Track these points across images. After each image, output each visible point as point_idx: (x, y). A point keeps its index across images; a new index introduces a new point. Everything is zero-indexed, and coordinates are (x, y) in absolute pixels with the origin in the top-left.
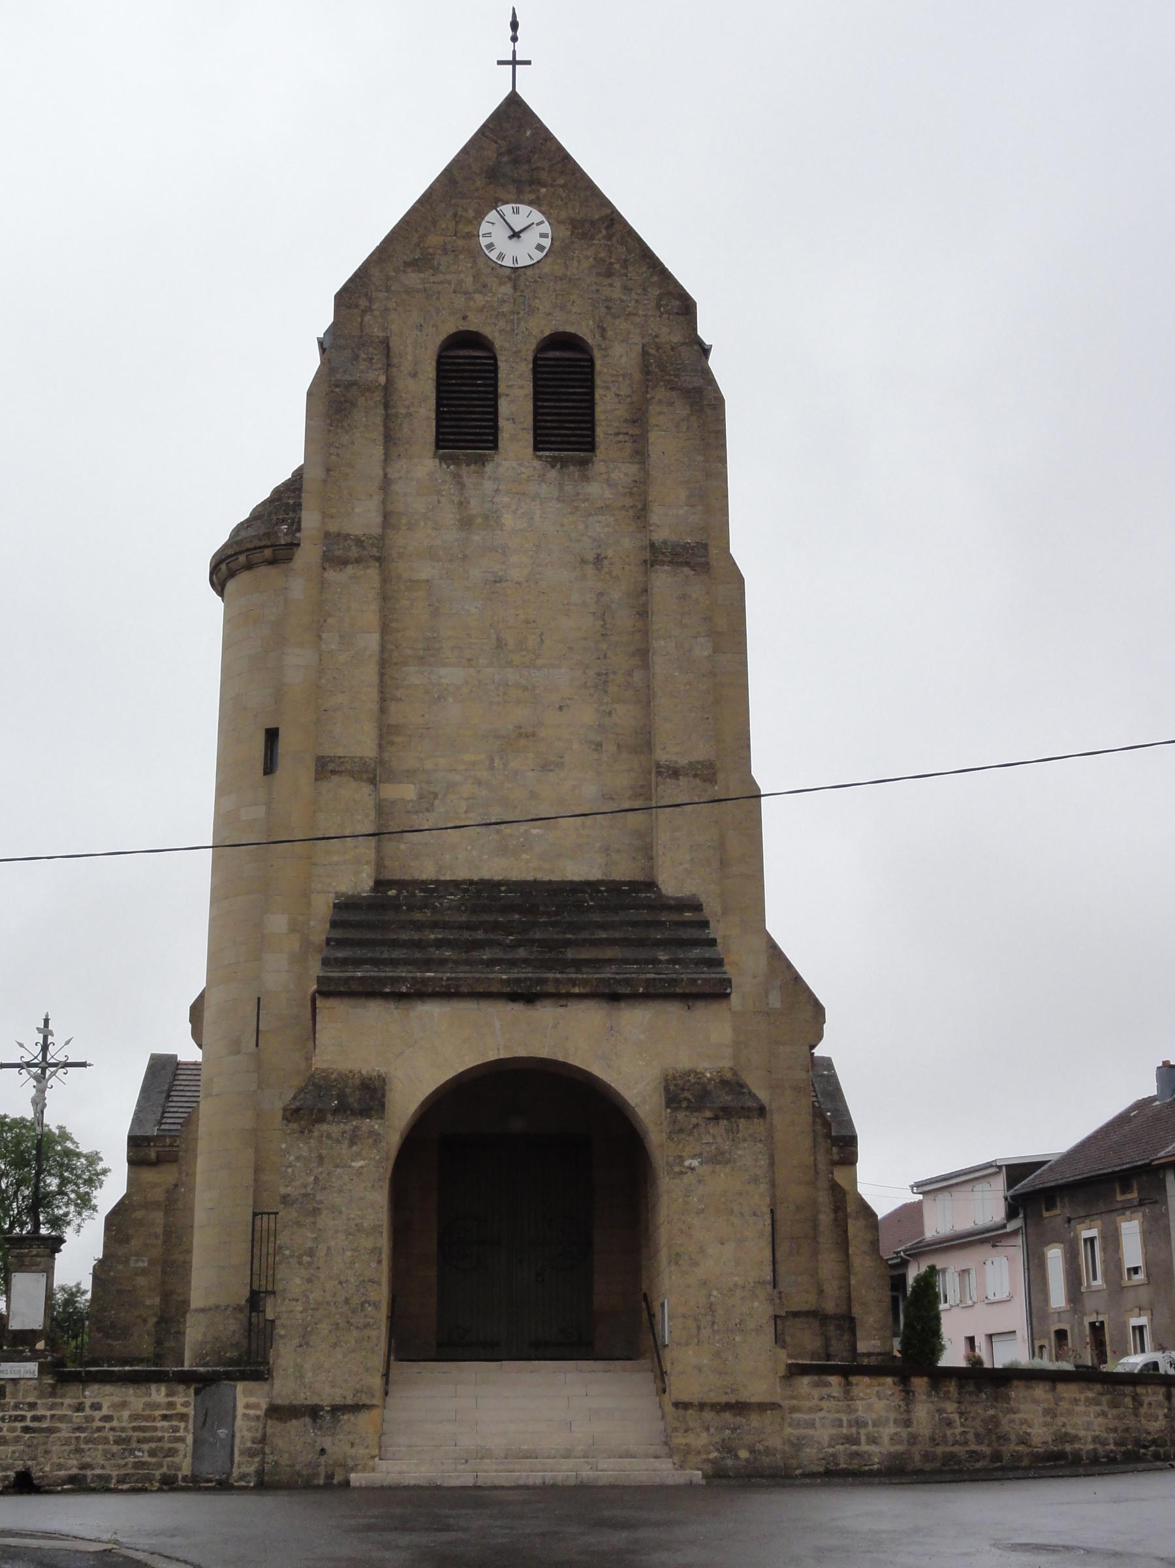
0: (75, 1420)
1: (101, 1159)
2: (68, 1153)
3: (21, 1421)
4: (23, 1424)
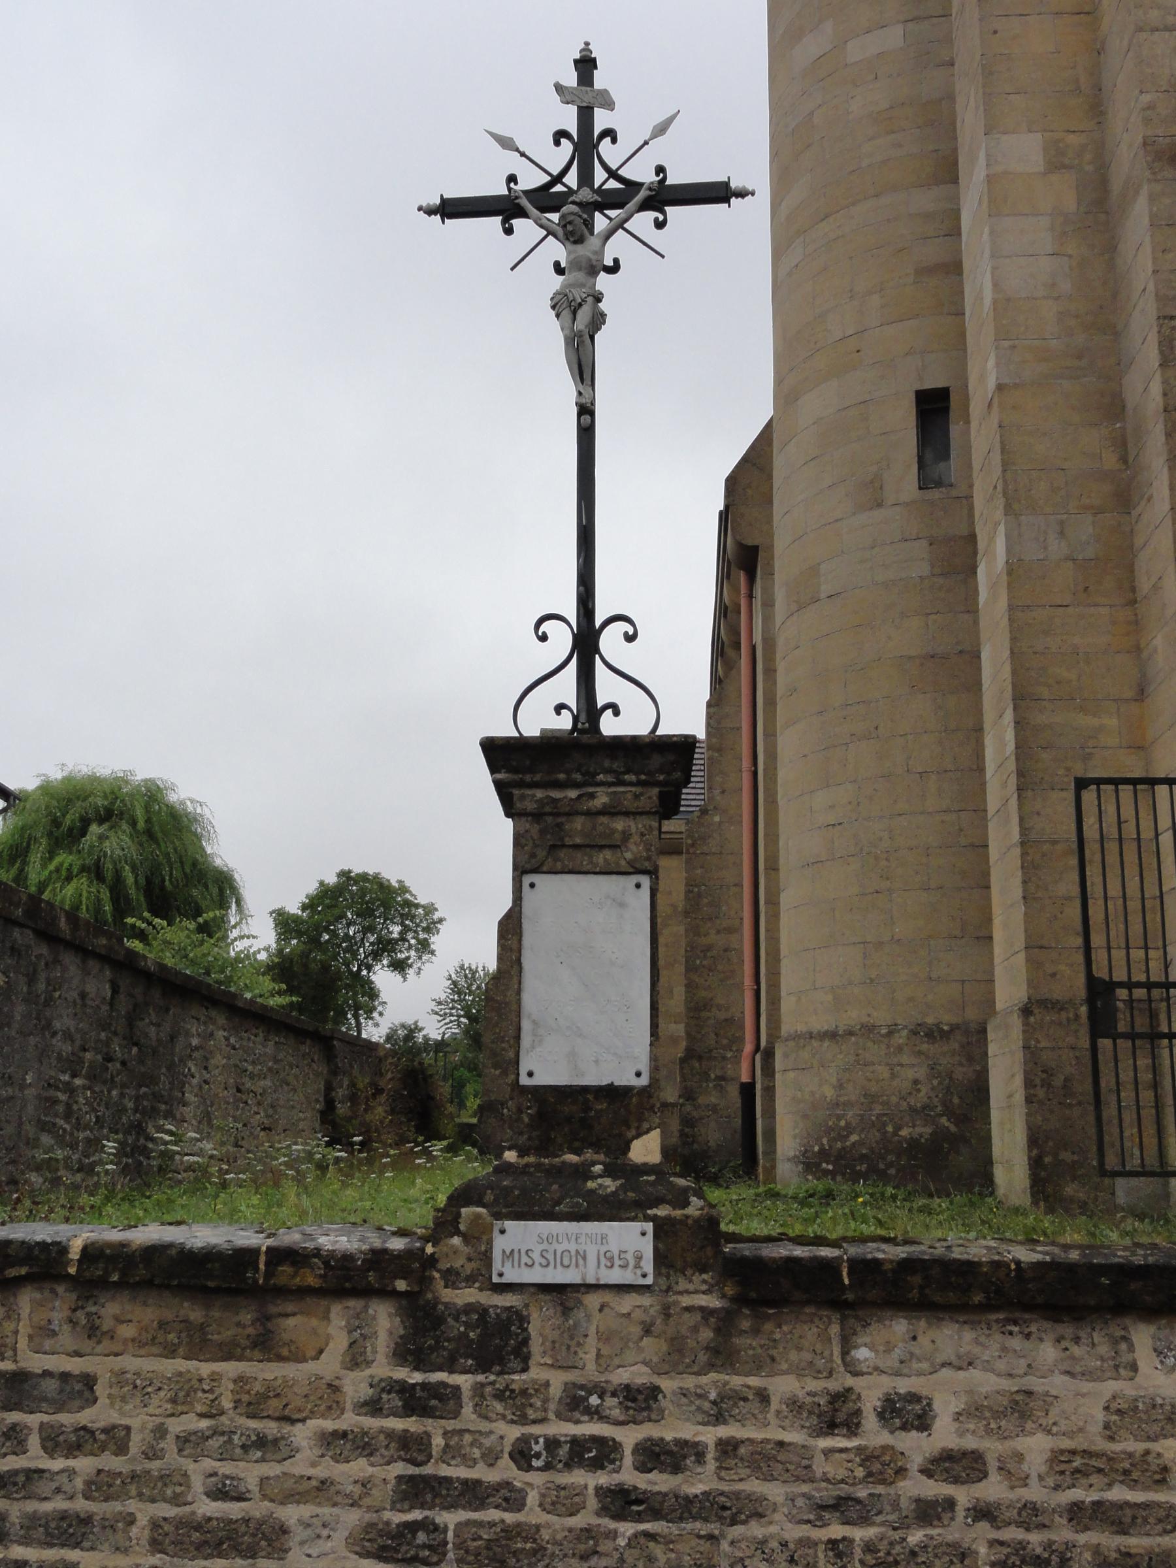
0: (820, 1466)
1: (436, 910)
2: (408, 904)
3: (597, 1465)
4: (603, 1479)
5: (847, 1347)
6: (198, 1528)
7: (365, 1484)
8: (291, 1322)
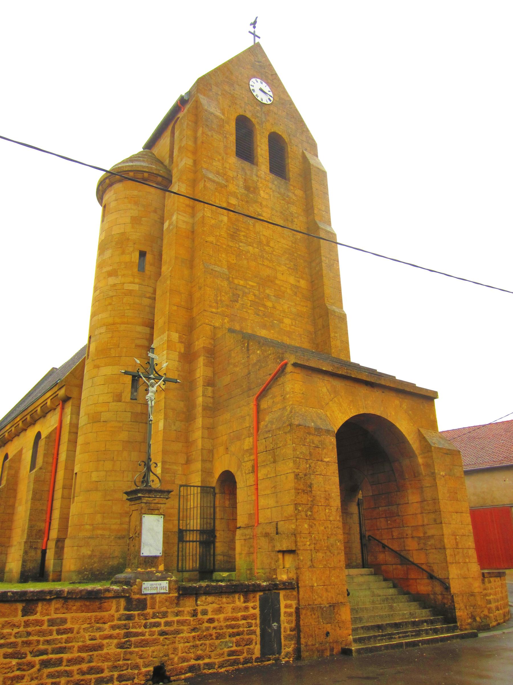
3: (157, 627)
5: (196, 601)
6: (87, 647)
7: (118, 634)
8: (105, 604)
